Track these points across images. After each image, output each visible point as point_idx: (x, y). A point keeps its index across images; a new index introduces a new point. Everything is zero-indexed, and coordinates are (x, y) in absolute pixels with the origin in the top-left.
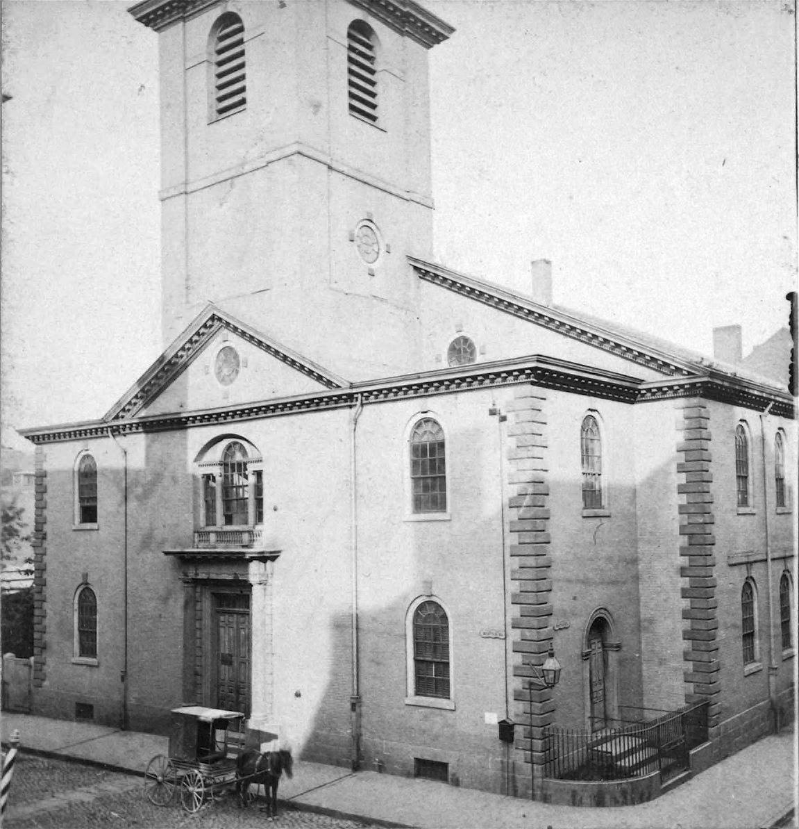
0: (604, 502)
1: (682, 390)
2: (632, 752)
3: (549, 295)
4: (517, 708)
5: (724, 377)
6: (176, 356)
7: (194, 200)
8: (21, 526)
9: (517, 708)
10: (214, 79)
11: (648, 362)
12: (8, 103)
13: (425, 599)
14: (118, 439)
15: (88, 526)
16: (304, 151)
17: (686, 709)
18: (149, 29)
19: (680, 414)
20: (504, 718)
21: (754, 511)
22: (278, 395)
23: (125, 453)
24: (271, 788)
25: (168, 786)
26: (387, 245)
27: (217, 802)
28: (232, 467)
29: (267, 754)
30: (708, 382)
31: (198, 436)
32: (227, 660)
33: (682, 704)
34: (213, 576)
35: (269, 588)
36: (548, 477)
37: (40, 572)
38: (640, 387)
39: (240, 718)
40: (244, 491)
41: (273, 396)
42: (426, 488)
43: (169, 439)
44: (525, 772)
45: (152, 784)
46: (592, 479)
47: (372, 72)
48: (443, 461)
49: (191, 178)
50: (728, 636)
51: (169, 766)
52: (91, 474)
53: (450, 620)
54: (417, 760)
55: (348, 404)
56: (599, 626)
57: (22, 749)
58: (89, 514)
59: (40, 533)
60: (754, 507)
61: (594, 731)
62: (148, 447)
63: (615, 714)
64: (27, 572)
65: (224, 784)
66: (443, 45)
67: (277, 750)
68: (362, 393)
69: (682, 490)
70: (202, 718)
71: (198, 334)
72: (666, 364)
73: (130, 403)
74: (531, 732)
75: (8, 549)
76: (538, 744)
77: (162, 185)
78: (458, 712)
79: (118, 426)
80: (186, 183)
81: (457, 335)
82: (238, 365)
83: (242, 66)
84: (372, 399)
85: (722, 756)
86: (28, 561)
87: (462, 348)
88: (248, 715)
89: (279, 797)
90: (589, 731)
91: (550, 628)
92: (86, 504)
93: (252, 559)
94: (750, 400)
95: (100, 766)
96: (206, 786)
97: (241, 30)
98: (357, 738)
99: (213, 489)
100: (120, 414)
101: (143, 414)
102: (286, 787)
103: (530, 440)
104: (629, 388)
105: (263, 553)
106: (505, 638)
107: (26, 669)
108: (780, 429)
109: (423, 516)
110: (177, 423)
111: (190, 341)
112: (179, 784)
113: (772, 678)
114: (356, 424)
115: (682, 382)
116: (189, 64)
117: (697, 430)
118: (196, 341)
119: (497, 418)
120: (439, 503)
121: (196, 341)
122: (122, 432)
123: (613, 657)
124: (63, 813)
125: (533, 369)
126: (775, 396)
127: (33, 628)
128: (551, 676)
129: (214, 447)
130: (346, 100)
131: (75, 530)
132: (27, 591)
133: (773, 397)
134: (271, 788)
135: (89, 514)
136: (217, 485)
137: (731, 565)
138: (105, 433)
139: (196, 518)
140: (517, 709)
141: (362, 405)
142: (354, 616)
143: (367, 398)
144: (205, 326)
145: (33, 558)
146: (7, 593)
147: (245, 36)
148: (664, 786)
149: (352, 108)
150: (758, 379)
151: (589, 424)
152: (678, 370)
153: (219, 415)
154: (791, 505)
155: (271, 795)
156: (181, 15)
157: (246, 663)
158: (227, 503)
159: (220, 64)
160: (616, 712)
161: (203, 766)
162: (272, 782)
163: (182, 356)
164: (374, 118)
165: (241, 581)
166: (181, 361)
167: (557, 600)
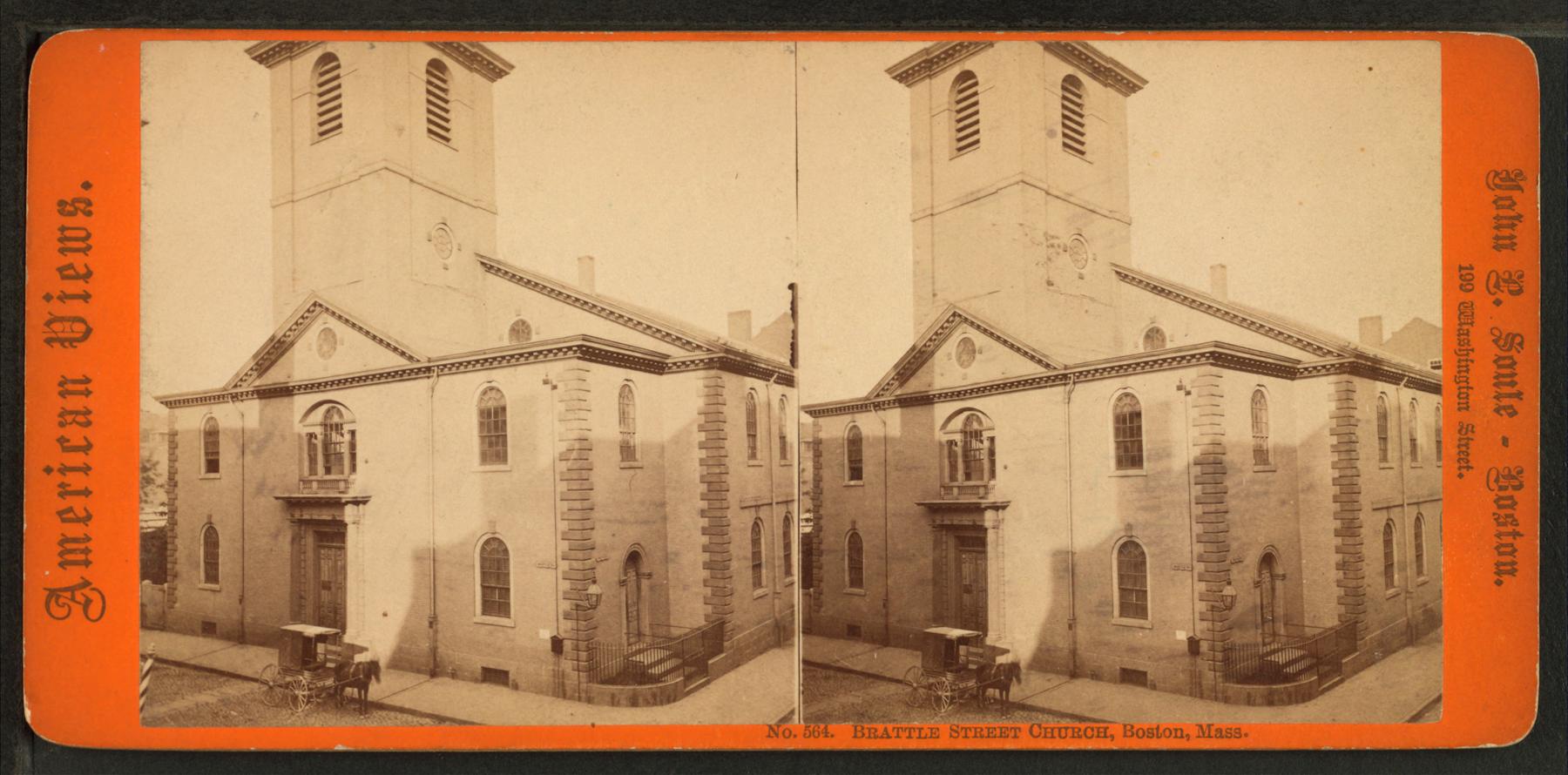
0: (638, 456)
1: (1333, 369)
2: (660, 662)
5: (737, 353)
8: (157, 475)
9: (1202, 626)
11: (674, 340)
14: (879, 412)
15: (212, 475)
16: (390, 167)
17: (705, 626)
19: (701, 383)
20: (1191, 634)
21: (1393, 465)
23: (243, 415)
24: (1004, 693)
26: (459, 245)
28: (971, 434)
29: (1001, 665)
30: (1354, 362)
31: (942, 410)
34: (315, 517)
35: (1000, 532)
36: (592, 435)
38: (667, 361)
39: (337, 634)
40: (340, 447)
42: (491, 444)
43: (918, 412)
44: (572, 678)
49: (936, 204)
50: (740, 566)
51: (923, 675)
52: (215, 433)
55: (427, 375)
56: (633, 558)
57: (157, 660)
58: (213, 466)
59: (172, 482)
60: (761, 460)
61: (629, 645)
62: (902, 414)
63: (647, 631)
64: (162, 514)
65: (324, 688)
66: (1139, 93)
67: (1009, 661)
68: (1074, 373)
69: (702, 446)
70: (948, 637)
71: (942, 327)
72: (689, 343)
73: (888, 384)
74: (577, 646)
75: (146, 494)
76: (583, 655)
78: (517, 629)
79: (879, 402)
80: (293, 193)
81: (517, 319)
84: (446, 371)
86: (163, 504)
87: (520, 329)
89: (369, 699)
90: (626, 645)
92: (210, 458)
93: (347, 503)
94: (759, 372)
95: (222, 673)
96: (309, 689)
98: (434, 650)
100: (239, 383)
105: (995, 503)
106: (556, 568)
107: (161, 593)
110: (925, 400)
113: (776, 601)
114: (433, 392)
115: (702, 357)
116: (934, 112)
117: (715, 398)
118: (939, 336)
119: (549, 386)
120: (502, 457)
121: (941, 334)
122: (240, 398)
124: (191, 712)
125: (1212, 353)
126: (779, 368)
127: (166, 560)
128: (594, 599)
129: (957, 417)
131: (845, 486)
132: (161, 530)
133: (1407, 374)
134: (1004, 693)
138: (226, 399)
139: (301, 470)
140: (566, 626)
141: (1074, 383)
142: (432, 552)
143: (442, 370)
145: (166, 502)
146: (145, 531)
148: (687, 689)
149: (1065, 145)
150: (765, 354)
151: (1258, 397)
154: (792, 458)
155: (363, 697)
156: (288, 54)
158: (327, 456)
159: (321, 95)
160: (648, 629)
163: (929, 346)
164: (447, 140)
167: (599, 536)
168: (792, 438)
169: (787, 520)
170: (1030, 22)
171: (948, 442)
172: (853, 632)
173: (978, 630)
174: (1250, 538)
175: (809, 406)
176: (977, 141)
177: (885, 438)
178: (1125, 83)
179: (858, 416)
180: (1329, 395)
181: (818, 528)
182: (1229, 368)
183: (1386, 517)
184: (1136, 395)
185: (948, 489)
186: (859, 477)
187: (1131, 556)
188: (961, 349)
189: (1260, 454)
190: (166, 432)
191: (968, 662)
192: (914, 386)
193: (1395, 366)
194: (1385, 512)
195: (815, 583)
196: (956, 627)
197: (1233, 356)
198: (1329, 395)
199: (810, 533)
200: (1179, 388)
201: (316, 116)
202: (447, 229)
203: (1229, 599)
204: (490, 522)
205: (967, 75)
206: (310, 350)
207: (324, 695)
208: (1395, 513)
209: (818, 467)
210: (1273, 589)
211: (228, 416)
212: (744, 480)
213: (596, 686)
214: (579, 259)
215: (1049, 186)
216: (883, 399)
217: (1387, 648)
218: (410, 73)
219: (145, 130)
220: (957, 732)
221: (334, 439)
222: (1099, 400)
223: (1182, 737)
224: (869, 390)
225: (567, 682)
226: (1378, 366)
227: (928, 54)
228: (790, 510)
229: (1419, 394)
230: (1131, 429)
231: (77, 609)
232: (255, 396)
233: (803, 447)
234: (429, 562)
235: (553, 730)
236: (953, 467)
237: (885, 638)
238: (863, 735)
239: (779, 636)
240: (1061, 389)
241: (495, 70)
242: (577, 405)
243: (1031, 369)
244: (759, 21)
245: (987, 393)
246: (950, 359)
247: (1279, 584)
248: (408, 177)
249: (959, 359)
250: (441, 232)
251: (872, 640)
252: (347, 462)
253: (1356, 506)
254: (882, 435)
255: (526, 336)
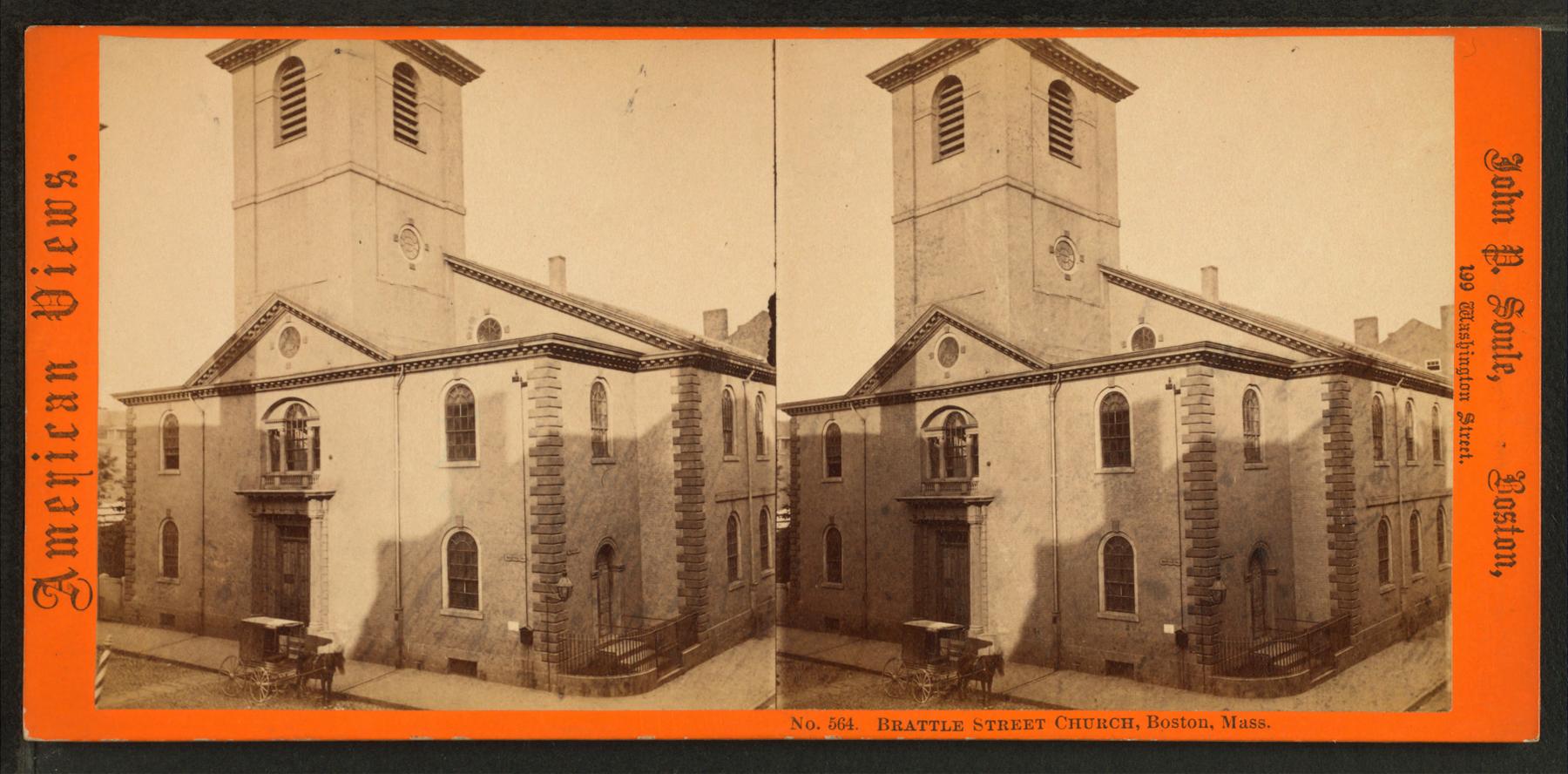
0: (611, 452)
2: (632, 653)
3: (563, 285)
4: (1191, 622)
5: (712, 351)
6: (247, 334)
7: (265, 211)
8: (114, 471)
9: (1191, 622)
10: (279, 111)
11: (637, 335)
12: (104, 131)
13: (457, 530)
14: (197, 401)
15: (834, 479)
16: (1013, 183)
18: (225, 71)
20: (525, 625)
21: (739, 459)
22: (333, 366)
23: (203, 413)
25: (901, 683)
26: (427, 245)
27: (280, 694)
28: (294, 423)
29: (323, 655)
31: (264, 400)
32: (289, 579)
33: (1328, 617)
34: (277, 512)
36: (563, 432)
37: (129, 505)
38: (641, 359)
39: (300, 626)
41: (986, 376)
42: (458, 441)
43: (239, 404)
45: (224, 679)
46: (1251, 440)
47: (1069, 121)
48: (473, 419)
49: (260, 191)
51: (240, 664)
53: (480, 548)
54: (1108, 662)
56: (606, 552)
57: (115, 651)
58: (172, 461)
59: (130, 481)
62: (882, 413)
63: (1273, 624)
64: (120, 509)
65: (286, 679)
66: (475, 82)
67: (332, 652)
68: (1060, 373)
69: (677, 442)
71: (265, 317)
72: (663, 341)
75: (104, 490)
77: (895, 211)
80: (256, 195)
81: (1141, 326)
82: (299, 341)
83: (304, 100)
84: (413, 368)
85: (709, 656)
86: (121, 499)
87: (490, 328)
88: (307, 622)
89: (993, 691)
91: (564, 553)
92: (170, 454)
93: (970, 504)
94: (728, 368)
96: (271, 680)
97: (303, 71)
99: (937, 450)
101: (878, 391)
102: (339, 681)
103: (1199, 409)
104: (1283, 367)
107: (119, 586)
108: (760, 392)
109: (1110, 470)
110: (245, 389)
111: (259, 323)
112: (248, 679)
113: (753, 593)
116: (258, 100)
117: (690, 395)
118: (264, 322)
119: (1172, 391)
123: (1270, 579)
124: (149, 703)
130: (391, 127)
132: (119, 524)
135: (172, 461)
136: (281, 438)
137: (718, 502)
141: (405, 374)
143: (1064, 376)
144: (271, 310)
147: (306, 76)
149: (397, 134)
150: (746, 352)
151: (598, 388)
152: (1323, 353)
153: (283, 382)
157: (305, 580)
158: (949, 461)
159: (285, 99)
161: (269, 665)
162: (328, 678)
165: (302, 516)
166: (911, 349)
167: (571, 532)
168: (769, 432)
169: (764, 513)
170: (1031, 18)
171: (270, 431)
172: (831, 625)
173: (299, 620)
174: (1234, 536)
175: (787, 405)
176: (304, 129)
177: (865, 435)
178: (463, 73)
179: (836, 415)
180: (672, 388)
181: (795, 524)
182: (568, 360)
183: (730, 511)
184: (1125, 394)
185: (269, 478)
186: (839, 474)
187: (462, 551)
188: (943, 350)
189: (599, 447)
190: (125, 428)
191: (949, 654)
192: (895, 385)
193: (741, 359)
194: (728, 505)
195: (127, 572)
196: (937, 620)
197: (572, 348)
198: (672, 388)
199: (788, 528)
200: (1169, 387)
201: (279, 119)
202: (1070, 243)
203: (565, 591)
204: (1113, 522)
205: (293, 62)
206: (272, 348)
207: (286, 686)
208: (1389, 511)
209: (795, 463)
210: (611, 583)
211: (188, 414)
212: (720, 475)
213: (567, 678)
214: (551, 260)
215: (379, 176)
216: (201, 388)
217: (1378, 643)
218: (376, 77)
219: (102, 133)
220: (980, 725)
221: (297, 436)
222: (1087, 396)
223: (1206, 727)
224: (186, 379)
225: (537, 673)
226: (723, 359)
227: (911, 59)
228: (767, 503)
229: (1417, 395)
230: (464, 420)
231: (65, 599)
232: (216, 394)
233: (780, 444)
234: (394, 555)
235: (477, 715)
236: (935, 465)
237: (865, 631)
238: (888, 728)
239: (755, 628)
240: (1046, 388)
241: (463, 73)
242: (550, 404)
243: (357, 359)
244: (759, 19)
245: (312, 383)
246: (272, 348)
247: (616, 576)
248: (372, 179)
249: (941, 359)
250: (407, 233)
251: (188, 630)
252: (310, 457)
253: (700, 498)
254: (862, 432)
255: (1149, 343)
